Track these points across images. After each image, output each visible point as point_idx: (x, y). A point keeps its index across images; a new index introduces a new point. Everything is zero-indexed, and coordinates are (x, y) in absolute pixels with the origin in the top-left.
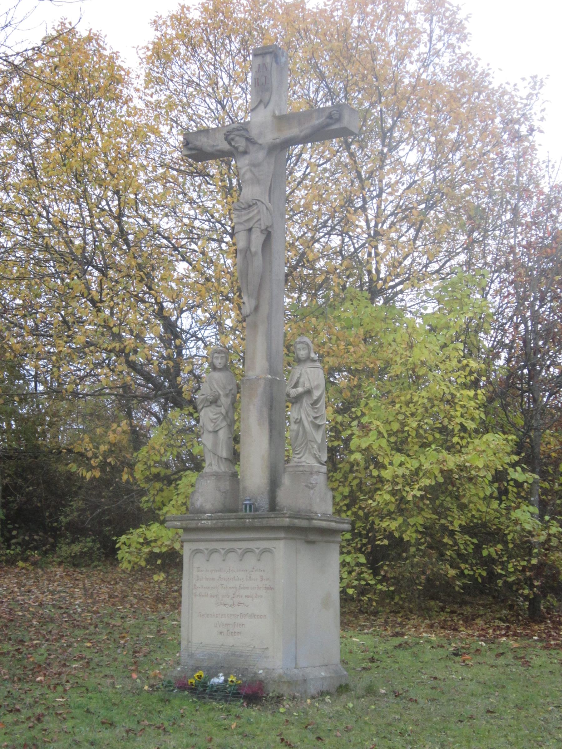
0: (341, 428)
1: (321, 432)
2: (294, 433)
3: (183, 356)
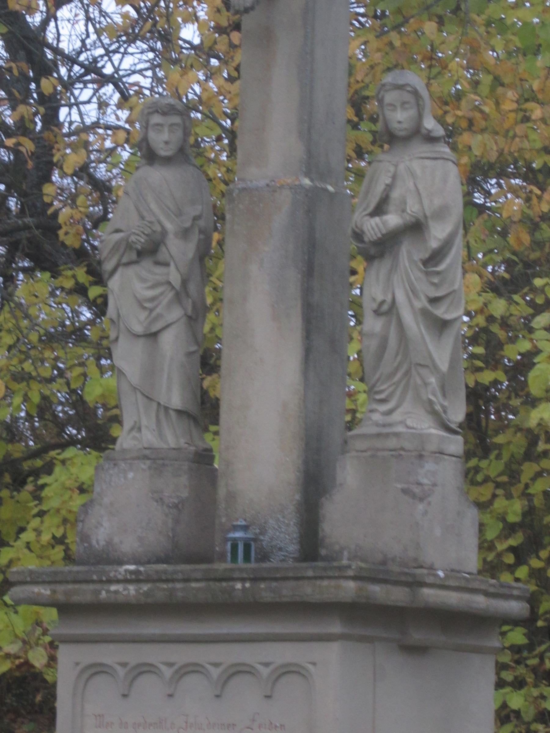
0: (501, 334)
1: (449, 341)
2: (373, 344)
3: (60, 125)
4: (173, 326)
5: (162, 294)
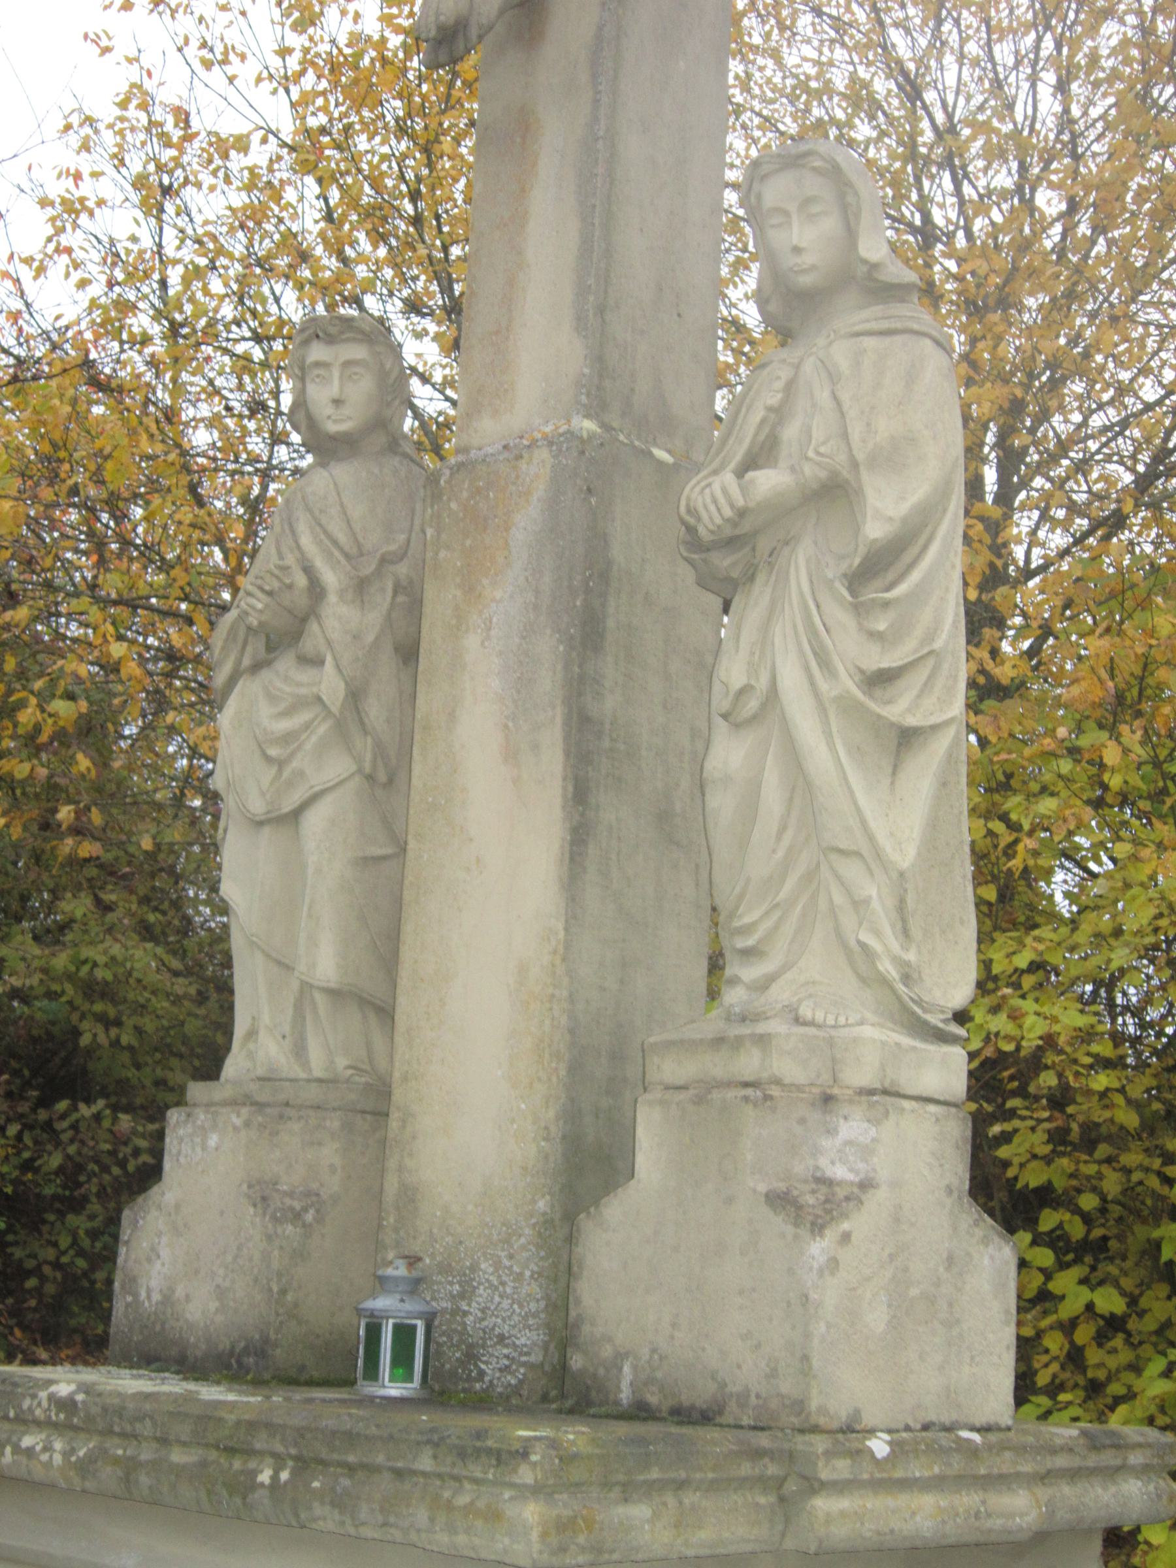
4: (328, 799)
5: (307, 726)
